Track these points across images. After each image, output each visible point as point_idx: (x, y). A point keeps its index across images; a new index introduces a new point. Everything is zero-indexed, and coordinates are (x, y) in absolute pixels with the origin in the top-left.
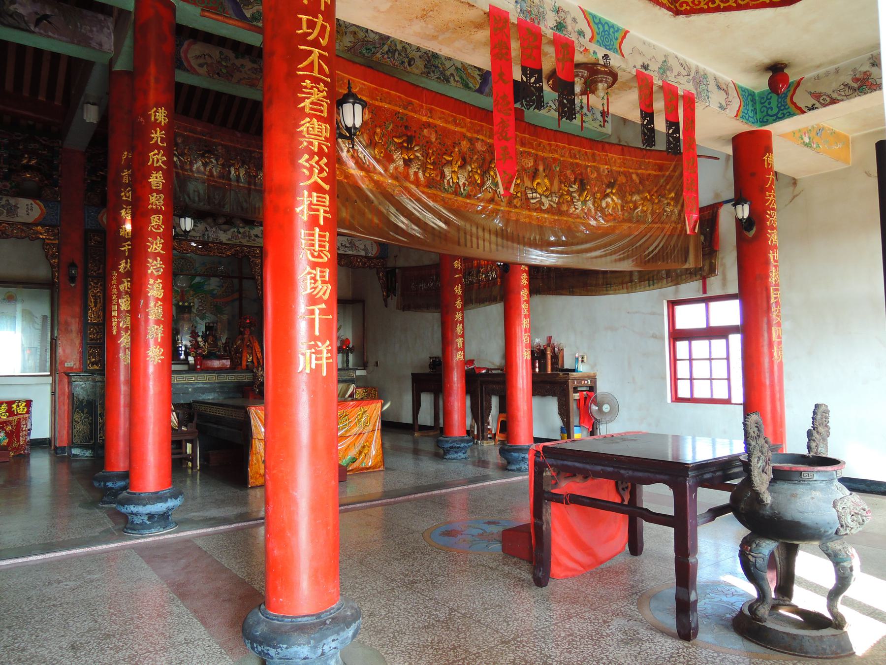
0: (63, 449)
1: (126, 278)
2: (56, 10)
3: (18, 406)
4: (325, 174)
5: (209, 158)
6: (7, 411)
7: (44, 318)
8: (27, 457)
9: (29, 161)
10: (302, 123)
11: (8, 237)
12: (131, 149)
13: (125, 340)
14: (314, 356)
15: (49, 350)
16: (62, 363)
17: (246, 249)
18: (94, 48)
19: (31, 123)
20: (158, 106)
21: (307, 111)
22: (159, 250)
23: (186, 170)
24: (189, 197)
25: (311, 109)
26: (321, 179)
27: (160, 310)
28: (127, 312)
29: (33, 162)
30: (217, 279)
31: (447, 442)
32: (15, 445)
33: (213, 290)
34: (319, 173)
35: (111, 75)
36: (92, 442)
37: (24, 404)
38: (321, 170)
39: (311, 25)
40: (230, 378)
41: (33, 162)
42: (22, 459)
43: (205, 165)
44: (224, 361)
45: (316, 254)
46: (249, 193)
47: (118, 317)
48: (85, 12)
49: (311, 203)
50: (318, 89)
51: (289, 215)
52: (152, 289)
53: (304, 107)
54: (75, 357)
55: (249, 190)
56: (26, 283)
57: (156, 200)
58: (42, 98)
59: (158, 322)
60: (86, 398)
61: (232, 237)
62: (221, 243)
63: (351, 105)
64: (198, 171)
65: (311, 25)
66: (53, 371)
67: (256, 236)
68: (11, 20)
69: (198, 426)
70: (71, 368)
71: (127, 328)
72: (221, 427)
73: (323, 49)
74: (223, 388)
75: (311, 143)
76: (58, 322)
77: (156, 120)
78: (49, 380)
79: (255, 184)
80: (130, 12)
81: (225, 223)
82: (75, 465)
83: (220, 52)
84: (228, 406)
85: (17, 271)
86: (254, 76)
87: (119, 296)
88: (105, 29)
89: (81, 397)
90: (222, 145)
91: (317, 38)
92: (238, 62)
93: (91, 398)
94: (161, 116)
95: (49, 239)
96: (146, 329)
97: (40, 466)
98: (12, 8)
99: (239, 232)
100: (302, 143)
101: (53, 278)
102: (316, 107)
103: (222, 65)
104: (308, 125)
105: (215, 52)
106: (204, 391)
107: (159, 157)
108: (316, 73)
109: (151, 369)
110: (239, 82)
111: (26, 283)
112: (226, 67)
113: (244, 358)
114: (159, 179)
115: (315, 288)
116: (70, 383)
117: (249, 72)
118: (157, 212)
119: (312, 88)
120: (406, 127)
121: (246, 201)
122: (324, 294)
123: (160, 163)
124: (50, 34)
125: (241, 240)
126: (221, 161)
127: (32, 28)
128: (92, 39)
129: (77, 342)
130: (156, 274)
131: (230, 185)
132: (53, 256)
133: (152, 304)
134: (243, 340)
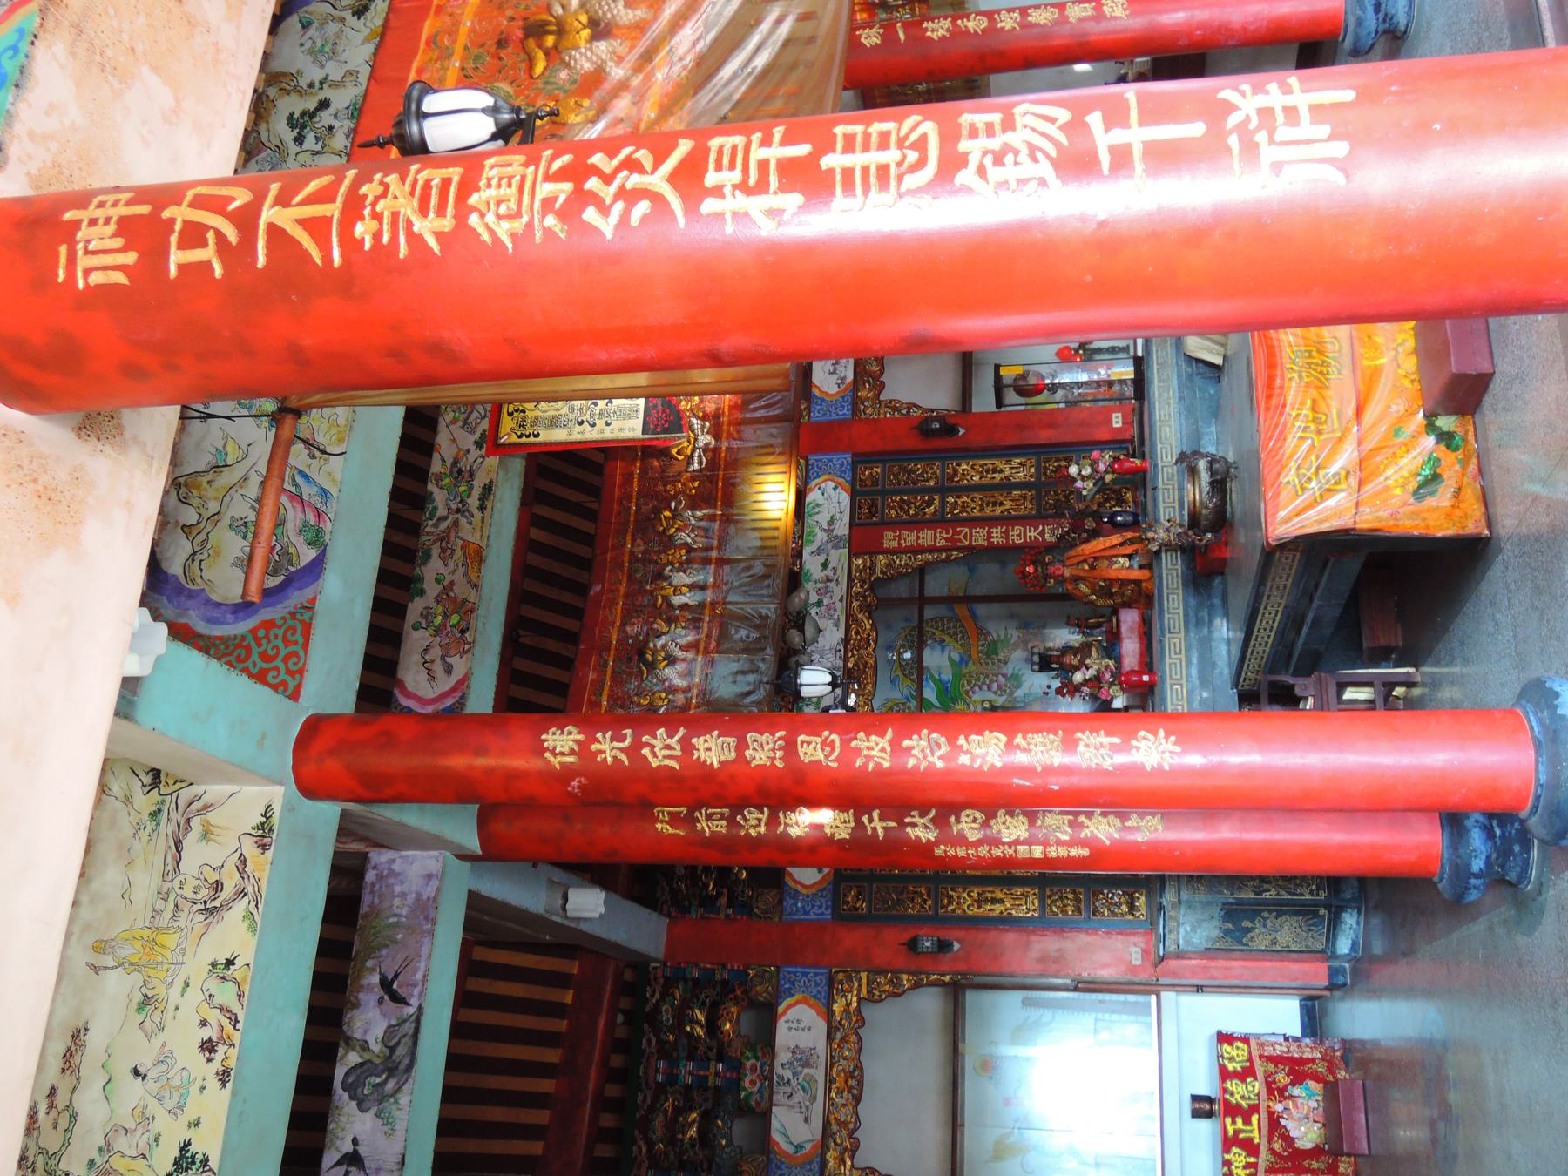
0: (1333, 972)
1: (949, 824)
2: (369, 963)
3: (1231, 1059)
4: (644, 156)
5: (655, 652)
6: (1243, 1080)
7: (1026, 1003)
8: (1348, 1046)
9: (698, 1022)
10: (486, 237)
11: (860, 1067)
12: (645, 808)
13: (1103, 829)
14: (1283, 133)
15: (1100, 996)
16: (1133, 969)
17: (856, 588)
18: (438, 890)
19: (620, 1018)
20: (540, 750)
21: (447, 223)
22: (884, 742)
23: (688, 700)
24: (749, 693)
25: (441, 212)
26: (658, 163)
27: (1038, 738)
28: (1032, 822)
29: (701, 1017)
30: (927, 653)
31: (1359, 22)
32: (1321, 1068)
33: (951, 660)
34: (642, 171)
35: (494, 852)
36: (1322, 911)
37: (1225, 1046)
38: (632, 165)
39: (194, 235)
40: (1174, 602)
41: (701, 1017)
42: (1354, 1054)
43: (671, 660)
44: (1124, 629)
45: (912, 156)
46: (728, 561)
47: (1046, 844)
48: (364, 909)
49: (743, 187)
50: (377, 199)
51: (785, 266)
52: (984, 757)
53: (438, 235)
54: (1119, 945)
55: (721, 562)
56: (955, 1034)
57: (763, 750)
58: (568, 997)
59: (1070, 744)
60: (1217, 922)
61: (830, 617)
62: (846, 641)
63: (428, 124)
64: (688, 674)
65: (194, 235)
66: (1149, 988)
67: (825, 565)
68: (401, 1051)
69: (1305, 670)
70: (1145, 952)
71: (1072, 824)
72: (1309, 619)
73: (259, 198)
74: (1197, 621)
75: (548, 203)
76: (1042, 975)
77: (572, 752)
78: (1167, 996)
79: (709, 548)
80: (344, 814)
81: (802, 630)
82: (1378, 948)
83: (415, 628)
84: (1257, 598)
85: (932, 1049)
86: (459, 553)
87: (997, 842)
88: (396, 867)
89: (1216, 933)
90: (623, 625)
91: (229, 217)
92: (432, 590)
93: (1217, 911)
94: (561, 743)
95: (859, 990)
96: (1088, 772)
97: (1367, 1019)
98: (376, 1047)
99: (819, 603)
100: (548, 232)
101: (944, 984)
102: (434, 201)
103: (443, 625)
104: (490, 218)
105: (416, 640)
106: (1207, 664)
107: (658, 744)
108: (333, 210)
109: (1195, 760)
110: (476, 586)
111: (955, 1034)
112: (446, 616)
113: (1123, 575)
114: (712, 744)
115: (1032, 149)
116: (1180, 955)
117: (452, 566)
118: (790, 747)
119: (377, 217)
120: (501, 44)
121: (749, 568)
122: (1052, 120)
123: (673, 742)
124: (419, 976)
125: (836, 598)
126: (660, 625)
127: (411, 1010)
128: (419, 895)
129: (1083, 938)
130: (944, 749)
131: (713, 604)
132: (895, 982)
133: (1021, 758)
134: (1076, 579)
